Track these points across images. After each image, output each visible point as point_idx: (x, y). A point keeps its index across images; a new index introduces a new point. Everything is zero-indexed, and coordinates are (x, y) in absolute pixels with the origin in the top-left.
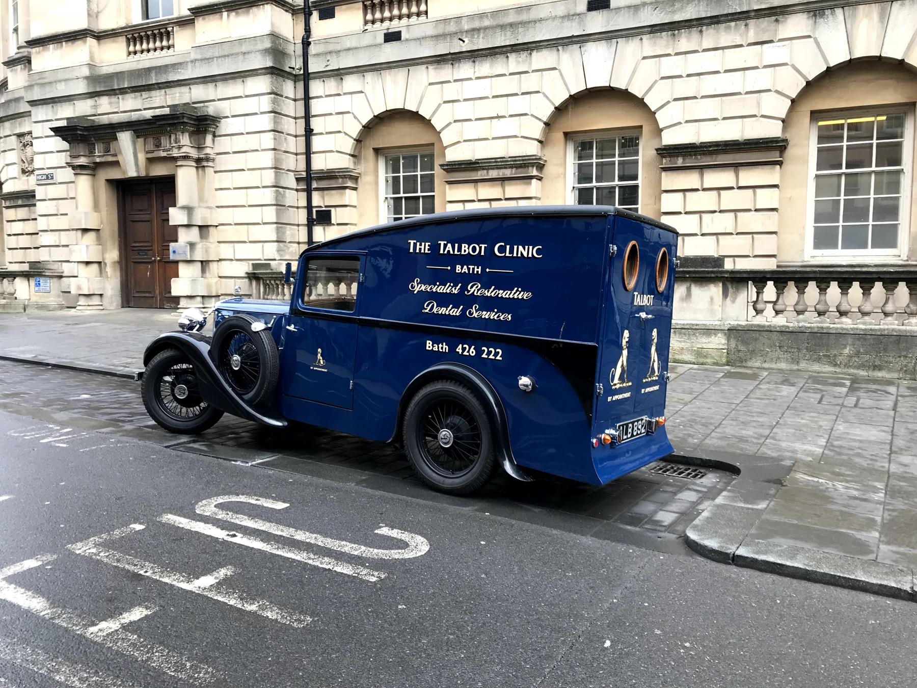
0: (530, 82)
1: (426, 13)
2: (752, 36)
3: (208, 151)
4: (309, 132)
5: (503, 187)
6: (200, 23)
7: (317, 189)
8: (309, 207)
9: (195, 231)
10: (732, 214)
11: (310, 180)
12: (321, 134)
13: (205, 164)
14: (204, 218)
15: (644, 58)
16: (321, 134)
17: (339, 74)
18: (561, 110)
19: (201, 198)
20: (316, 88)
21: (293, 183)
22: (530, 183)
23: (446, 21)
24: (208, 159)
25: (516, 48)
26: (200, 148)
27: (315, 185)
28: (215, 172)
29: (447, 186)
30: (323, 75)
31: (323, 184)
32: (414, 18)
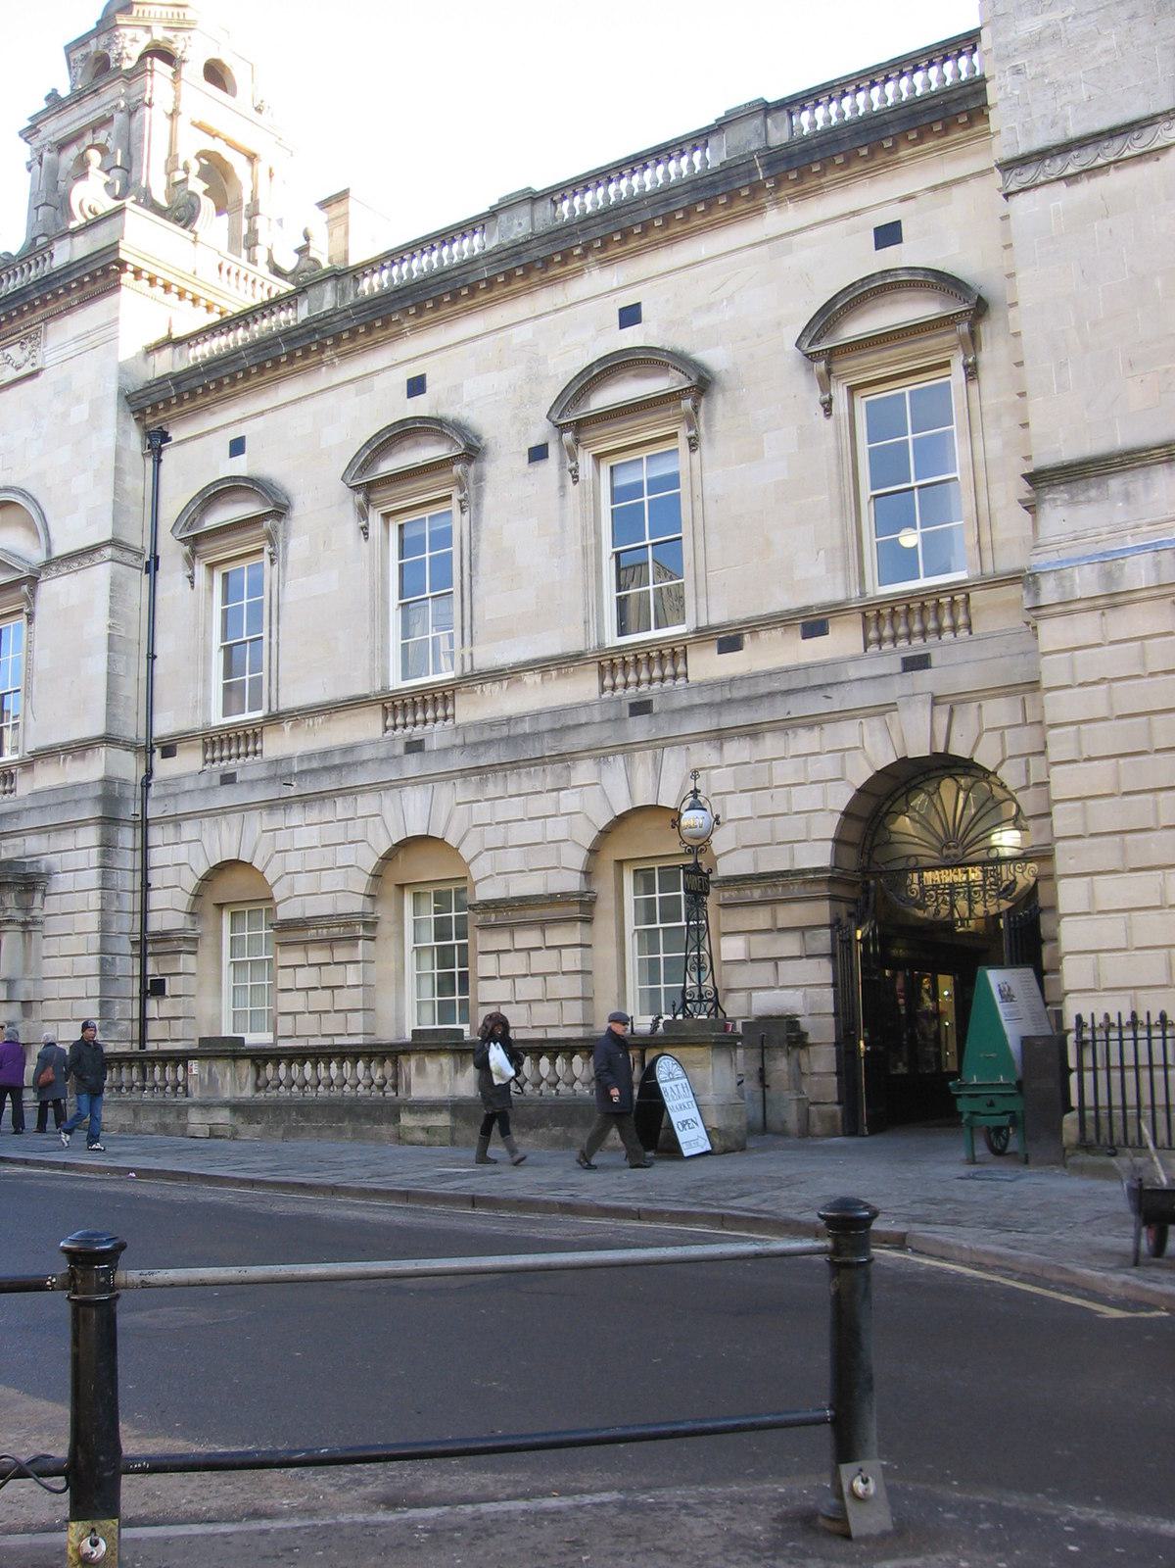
0: (356, 830)
1: (454, 716)
2: (549, 783)
3: (35, 913)
4: (146, 886)
5: (306, 951)
6: (39, 768)
7: (152, 954)
8: (143, 976)
9: (16, 1008)
10: (541, 979)
11: (146, 943)
12: (159, 889)
13: (31, 928)
14: (27, 993)
15: (458, 804)
16: (159, 889)
17: (176, 820)
18: (387, 858)
19: (26, 969)
20: (156, 835)
21: (128, 948)
22: (357, 945)
23: (277, 761)
24: (35, 923)
25: (342, 792)
26: (27, 909)
27: (150, 949)
28: (44, 937)
29: (721, 911)
30: (162, 821)
31: (160, 948)
32: (668, 683)
